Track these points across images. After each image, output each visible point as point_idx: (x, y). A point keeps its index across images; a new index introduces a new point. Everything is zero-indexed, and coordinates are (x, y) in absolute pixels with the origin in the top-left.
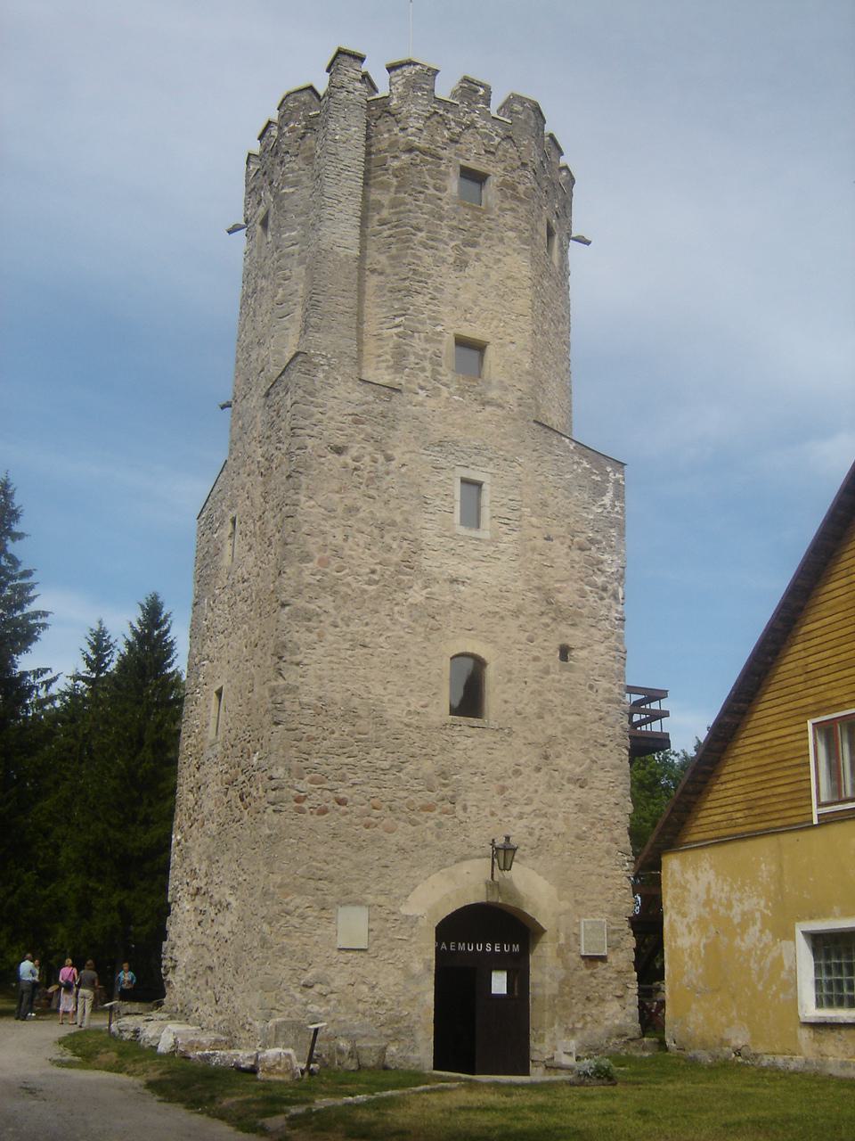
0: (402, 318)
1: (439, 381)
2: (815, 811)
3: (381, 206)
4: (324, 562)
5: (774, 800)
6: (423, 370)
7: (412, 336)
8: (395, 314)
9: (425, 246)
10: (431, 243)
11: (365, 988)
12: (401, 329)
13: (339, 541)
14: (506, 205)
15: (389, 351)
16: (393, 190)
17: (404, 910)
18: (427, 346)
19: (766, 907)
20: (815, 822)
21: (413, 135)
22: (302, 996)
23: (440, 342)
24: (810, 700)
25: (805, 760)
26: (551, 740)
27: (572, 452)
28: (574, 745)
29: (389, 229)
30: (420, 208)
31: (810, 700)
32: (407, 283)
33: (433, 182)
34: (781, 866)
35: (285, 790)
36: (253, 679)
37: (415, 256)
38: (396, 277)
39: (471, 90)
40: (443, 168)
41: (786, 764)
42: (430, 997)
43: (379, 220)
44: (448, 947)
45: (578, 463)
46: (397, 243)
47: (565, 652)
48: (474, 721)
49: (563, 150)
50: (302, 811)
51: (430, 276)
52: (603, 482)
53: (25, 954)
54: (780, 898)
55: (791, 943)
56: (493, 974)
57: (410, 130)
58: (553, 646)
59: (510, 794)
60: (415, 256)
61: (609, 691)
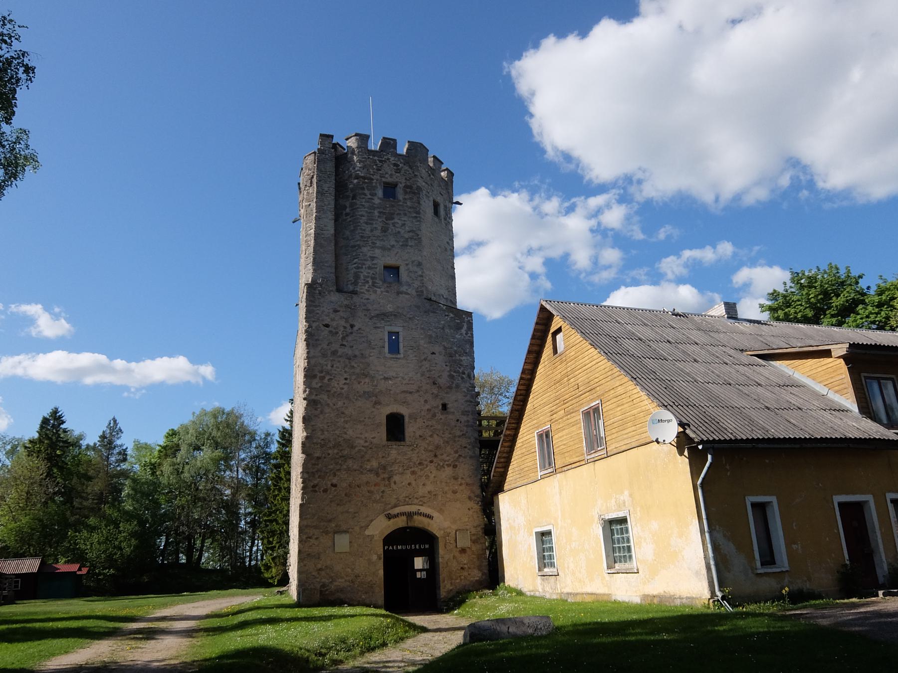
0: (357, 260)
1: (375, 286)
3: (345, 207)
4: (322, 378)
6: (368, 282)
7: (362, 268)
9: (366, 223)
10: (369, 221)
11: (349, 570)
13: (329, 367)
14: (407, 197)
16: (351, 199)
17: (367, 533)
18: (369, 271)
23: (376, 268)
25: (495, 474)
26: (438, 447)
27: (445, 310)
30: (363, 205)
32: (358, 243)
33: (369, 192)
36: (183, 509)
37: (361, 229)
39: (389, 144)
40: (374, 184)
42: (381, 572)
43: (346, 214)
44: (393, 548)
45: (448, 316)
47: (444, 406)
48: (402, 443)
49: (442, 160)
50: (315, 491)
51: (369, 237)
52: (461, 323)
56: (415, 558)
57: (356, 169)
58: (439, 403)
59: (791, 287)
60: (361, 229)
61: (468, 421)
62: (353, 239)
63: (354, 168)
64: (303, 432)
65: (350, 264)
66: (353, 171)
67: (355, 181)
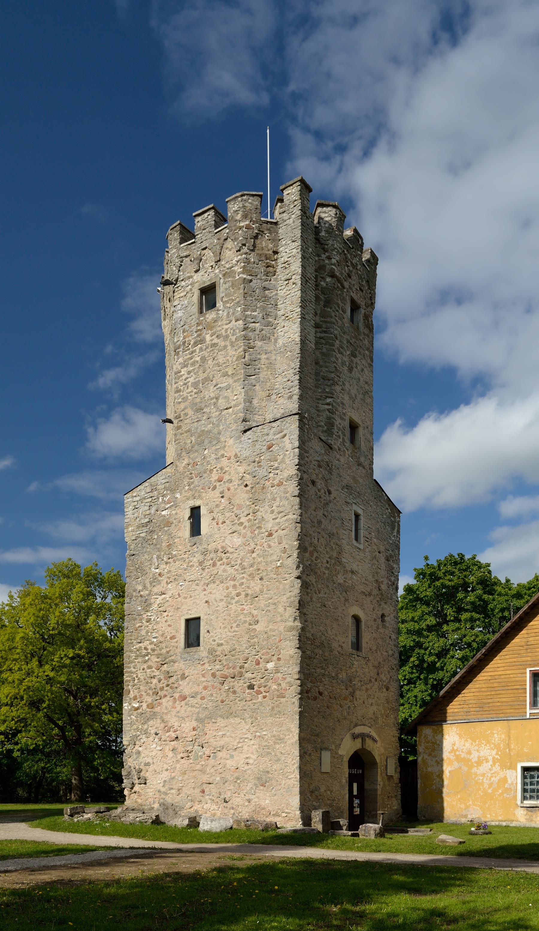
2: (528, 711)
5: (499, 704)
8: (327, 395)
12: (330, 407)
15: (324, 420)
19: (497, 754)
20: (528, 717)
21: (334, 265)
22: (313, 341)
24: (529, 659)
28: (151, 794)
29: (320, 332)
31: (529, 659)
34: (509, 736)
35: (218, 487)
38: (326, 369)
41: (509, 688)
46: (326, 344)
53: (96, 750)
54: (507, 750)
55: (514, 771)
62: (327, 367)
63: (329, 258)
64: (295, 619)
65: (321, 402)
66: (327, 261)
67: (328, 279)
